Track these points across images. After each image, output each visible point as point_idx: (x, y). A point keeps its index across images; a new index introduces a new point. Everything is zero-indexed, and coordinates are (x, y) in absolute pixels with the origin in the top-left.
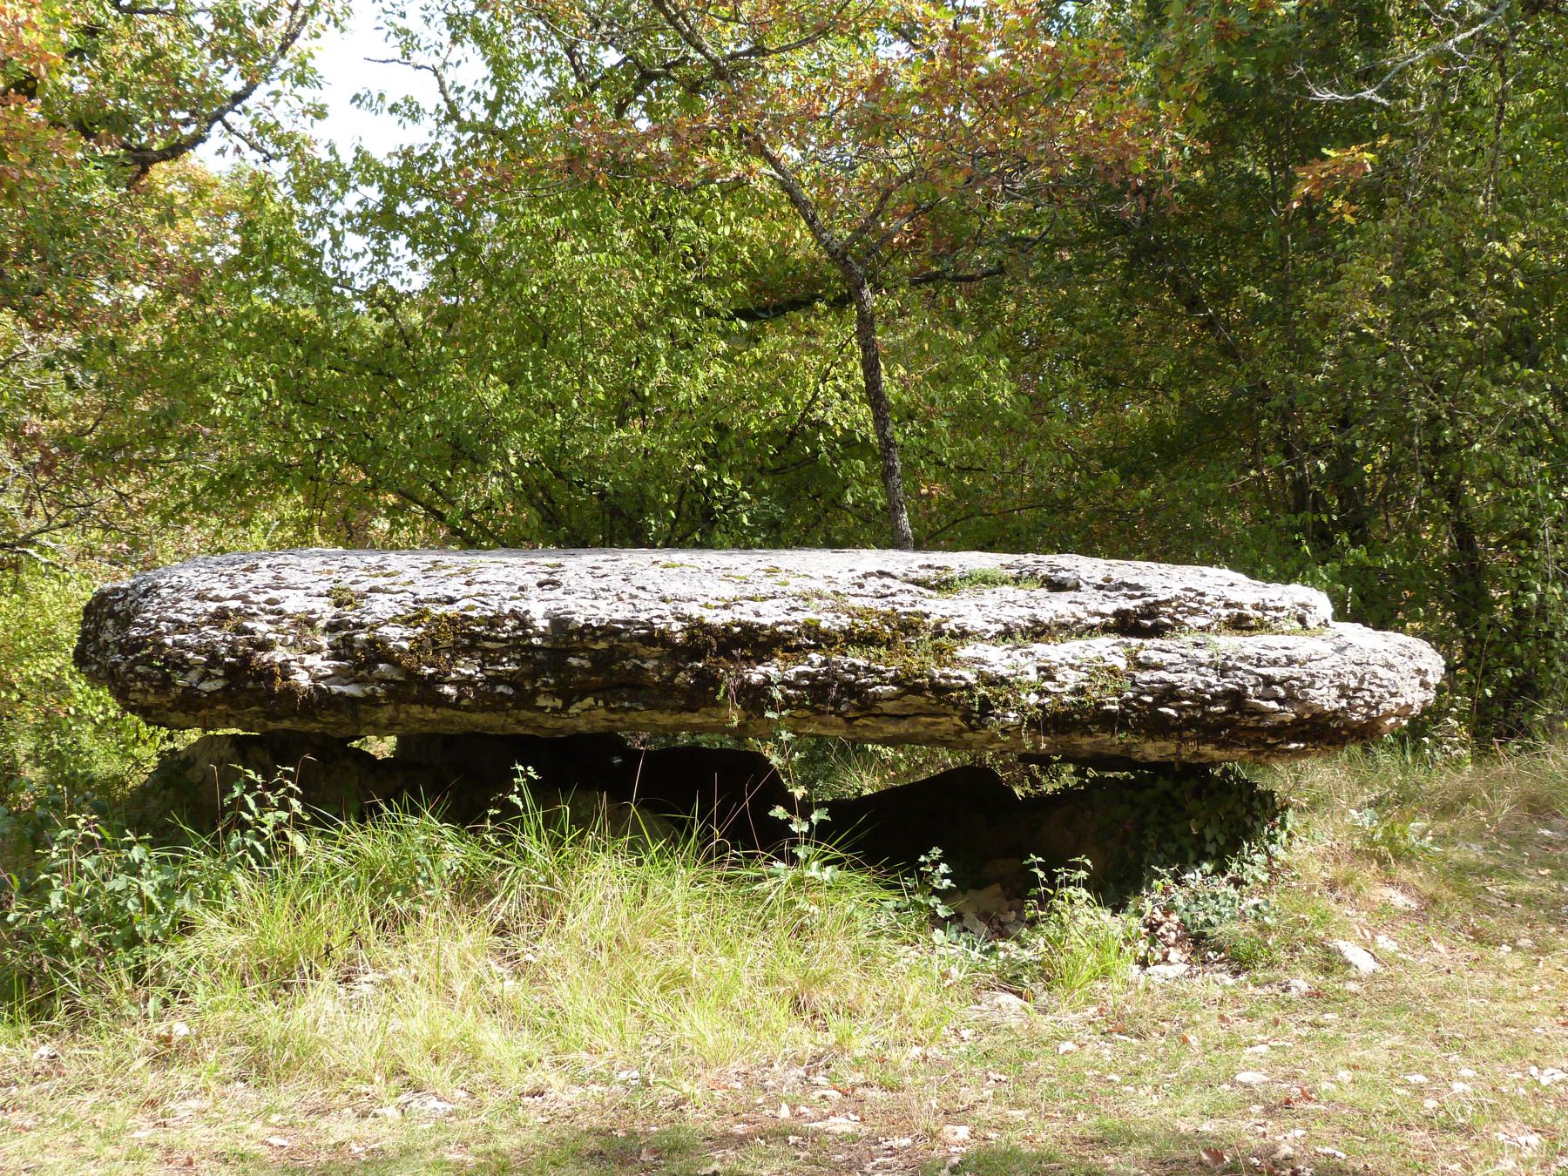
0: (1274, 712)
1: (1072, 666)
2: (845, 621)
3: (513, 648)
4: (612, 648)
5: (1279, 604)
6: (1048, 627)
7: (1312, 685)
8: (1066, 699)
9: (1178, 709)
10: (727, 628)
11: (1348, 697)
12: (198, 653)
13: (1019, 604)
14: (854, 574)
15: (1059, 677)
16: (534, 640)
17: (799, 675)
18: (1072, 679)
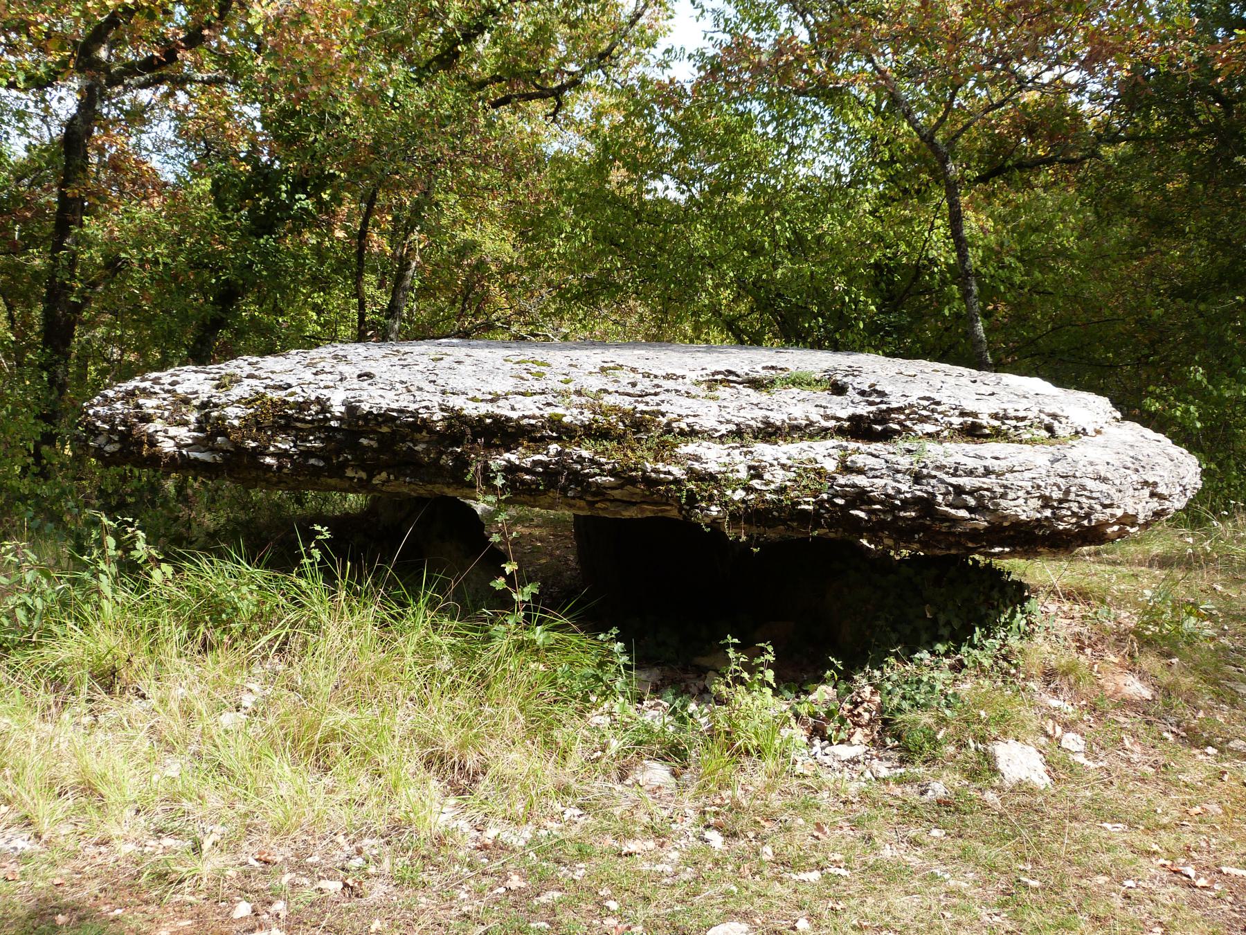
0: (963, 519)
1: (783, 466)
2: (587, 416)
3: (319, 429)
4: (393, 433)
5: (1021, 414)
6: (779, 428)
7: (1004, 496)
8: (768, 496)
9: (869, 512)
10: (481, 419)
11: (1052, 507)
12: (104, 422)
13: (747, 408)
14: (704, 372)
15: (767, 476)
16: (332, 423)
17: (535, 463)
18: (779, 477)
